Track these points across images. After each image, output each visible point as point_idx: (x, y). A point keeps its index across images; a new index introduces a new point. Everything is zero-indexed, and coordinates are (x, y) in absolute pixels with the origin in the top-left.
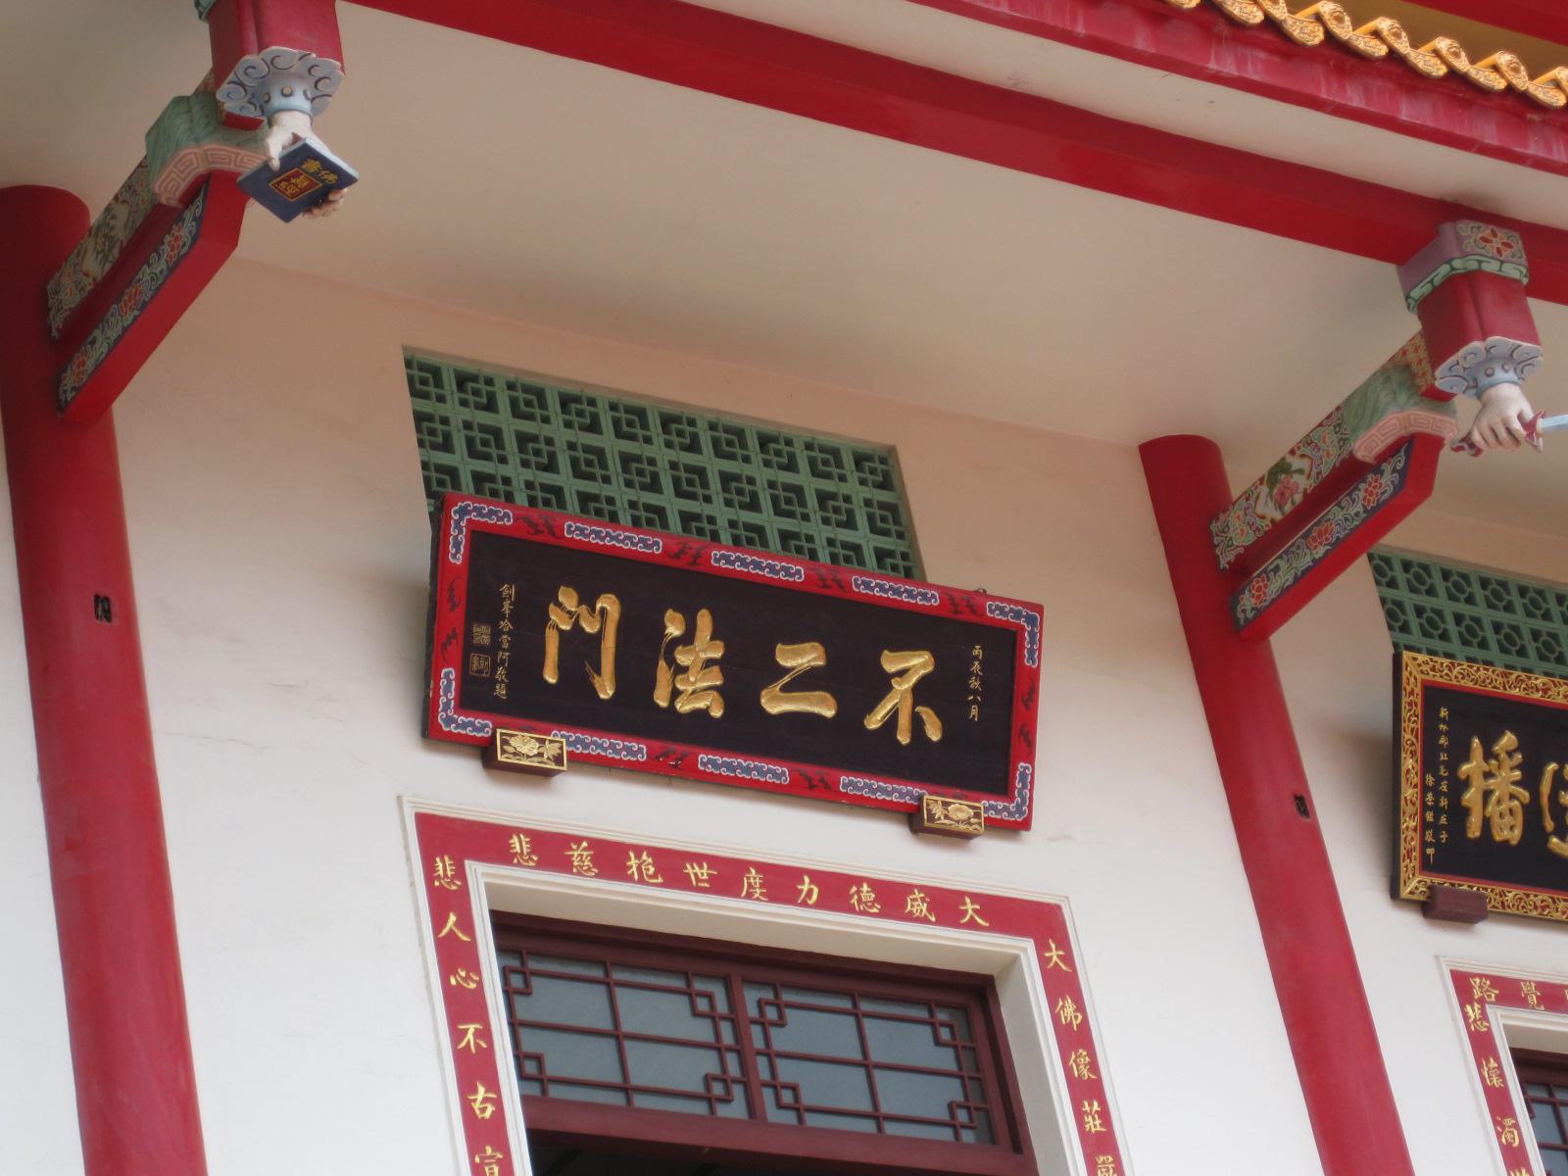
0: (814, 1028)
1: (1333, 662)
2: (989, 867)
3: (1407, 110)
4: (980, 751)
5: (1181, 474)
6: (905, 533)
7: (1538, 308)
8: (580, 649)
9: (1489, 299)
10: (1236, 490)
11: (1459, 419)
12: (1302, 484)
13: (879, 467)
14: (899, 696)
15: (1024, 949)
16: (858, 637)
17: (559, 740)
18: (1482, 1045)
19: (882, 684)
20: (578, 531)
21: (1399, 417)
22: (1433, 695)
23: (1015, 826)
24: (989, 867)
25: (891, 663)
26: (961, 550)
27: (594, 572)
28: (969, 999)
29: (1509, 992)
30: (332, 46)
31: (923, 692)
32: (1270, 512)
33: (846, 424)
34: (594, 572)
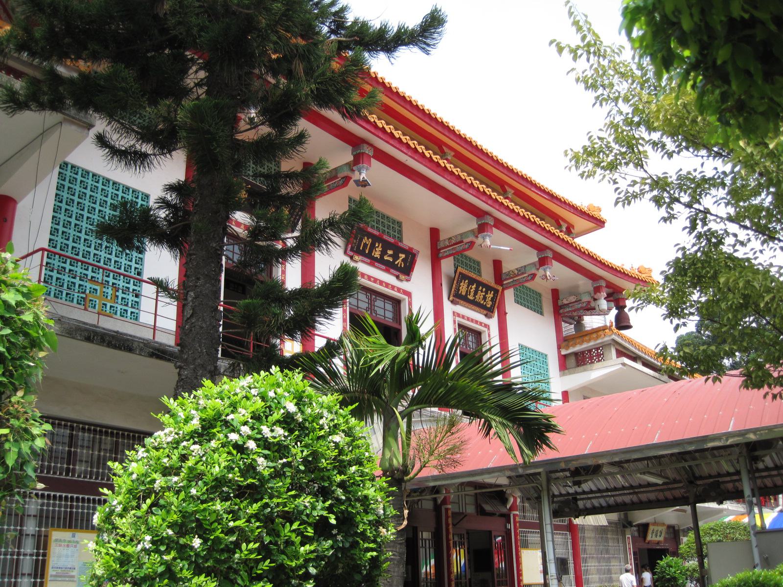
0: (379, 303)
1: (447, 266)
2: (404, 285)
3: (391, 142)
4: (406, 270)
5: (434, 233)
6: (401, 235)
7: (373, 161)
8: (365, 245)
9: (365, 157)
10: (441, 239)
11: (479, 241)
12: (453, 242)
13: (400, 224)
14: (399, 261)
15: (406, 298)
16: (398, 250)
17: (361, 258)
18: (455, 322)
19: (398, 258)
20: (370, 230)
21: (471, 238)
22: (460, 273)
23: (408, 280)
24: (404, 285)
25: (400, 255)
26: (409, 241)
27: (370, 235)
28: (397, 303)
29: (459, 315)
30: (370, 165)
31: (403, 260)
32: (447, 243)
33: (397, 217)
34: (370, 235)
